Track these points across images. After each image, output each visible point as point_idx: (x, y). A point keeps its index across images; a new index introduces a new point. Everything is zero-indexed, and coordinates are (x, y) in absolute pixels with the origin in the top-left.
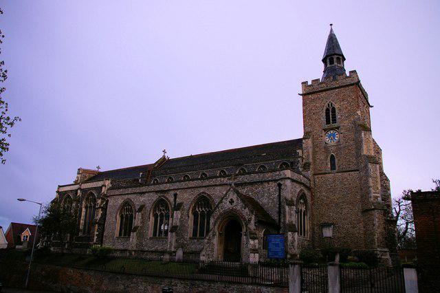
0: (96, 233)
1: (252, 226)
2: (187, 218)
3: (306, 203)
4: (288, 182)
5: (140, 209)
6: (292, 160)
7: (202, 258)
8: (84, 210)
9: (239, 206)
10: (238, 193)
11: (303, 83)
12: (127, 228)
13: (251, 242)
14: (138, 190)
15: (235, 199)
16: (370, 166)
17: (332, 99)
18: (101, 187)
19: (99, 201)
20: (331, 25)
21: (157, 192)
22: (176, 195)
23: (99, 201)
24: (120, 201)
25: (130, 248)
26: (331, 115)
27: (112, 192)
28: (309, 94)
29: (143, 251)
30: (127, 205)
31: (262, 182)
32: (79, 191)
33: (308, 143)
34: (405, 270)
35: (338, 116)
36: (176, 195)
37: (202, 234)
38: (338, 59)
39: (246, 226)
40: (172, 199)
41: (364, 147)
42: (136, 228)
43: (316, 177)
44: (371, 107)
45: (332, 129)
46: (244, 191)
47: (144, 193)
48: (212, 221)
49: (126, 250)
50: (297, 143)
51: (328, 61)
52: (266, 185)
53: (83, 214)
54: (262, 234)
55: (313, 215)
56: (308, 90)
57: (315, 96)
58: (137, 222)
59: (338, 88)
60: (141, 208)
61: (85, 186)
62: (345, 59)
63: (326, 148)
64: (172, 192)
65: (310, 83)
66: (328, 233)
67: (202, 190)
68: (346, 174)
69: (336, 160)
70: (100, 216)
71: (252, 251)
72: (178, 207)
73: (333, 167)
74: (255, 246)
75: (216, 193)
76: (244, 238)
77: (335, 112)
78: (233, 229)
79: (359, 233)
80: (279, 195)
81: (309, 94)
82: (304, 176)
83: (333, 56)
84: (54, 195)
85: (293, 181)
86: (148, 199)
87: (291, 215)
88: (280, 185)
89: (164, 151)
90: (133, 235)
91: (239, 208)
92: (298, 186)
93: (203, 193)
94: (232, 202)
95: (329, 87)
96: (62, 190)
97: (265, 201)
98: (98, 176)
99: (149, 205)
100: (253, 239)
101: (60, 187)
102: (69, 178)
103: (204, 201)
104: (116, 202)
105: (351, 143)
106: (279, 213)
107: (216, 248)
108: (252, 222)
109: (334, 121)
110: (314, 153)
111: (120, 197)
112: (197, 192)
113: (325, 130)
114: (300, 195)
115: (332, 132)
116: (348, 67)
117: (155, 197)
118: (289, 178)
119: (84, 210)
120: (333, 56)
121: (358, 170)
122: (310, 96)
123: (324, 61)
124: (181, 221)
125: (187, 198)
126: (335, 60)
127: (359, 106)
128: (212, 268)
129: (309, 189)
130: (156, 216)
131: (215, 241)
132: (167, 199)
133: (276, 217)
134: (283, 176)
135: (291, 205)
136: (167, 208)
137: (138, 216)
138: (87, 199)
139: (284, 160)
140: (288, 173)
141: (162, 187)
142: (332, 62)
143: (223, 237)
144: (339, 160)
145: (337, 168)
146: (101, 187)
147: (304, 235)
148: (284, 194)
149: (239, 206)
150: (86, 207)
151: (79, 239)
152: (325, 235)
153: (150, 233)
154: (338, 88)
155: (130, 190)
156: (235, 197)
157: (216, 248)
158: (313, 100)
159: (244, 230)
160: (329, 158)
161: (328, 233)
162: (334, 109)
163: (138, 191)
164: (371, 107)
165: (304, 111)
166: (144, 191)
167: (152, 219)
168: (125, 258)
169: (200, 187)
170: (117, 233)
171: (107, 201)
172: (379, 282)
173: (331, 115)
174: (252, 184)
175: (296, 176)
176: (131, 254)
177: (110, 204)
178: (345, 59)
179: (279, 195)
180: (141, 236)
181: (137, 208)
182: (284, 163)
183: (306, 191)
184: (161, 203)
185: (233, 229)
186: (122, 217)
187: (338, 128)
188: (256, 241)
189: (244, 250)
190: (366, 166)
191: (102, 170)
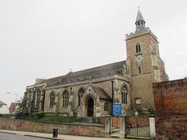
0: (41, 106)
1: (98, 100)
2: (76, 98)
3: (127, 89)
4: (116, 80)
5: (57, 95)
6: (121, 70)
7: (78, 115)
8: (36, 96)
9: (92, 92)
10: (92, 87)
11: (126, 35)
12: (52, 103)
13: (97, 108)
14: (56, 87)
15: (91, 89)
16: (155, 70)
17: (138, 41)
18: (42, 86)
19: (42, 92)
20: (139, 7)
21: (64, 87)
22: (71, 88)
23: (42, 92)
24: (50, 92)
25: (53, 112)
26: (138, 48)
27: (47, 88)
28: (129, 39)
29: (59, 113)
30: (52, 94)
31: (105, 81)
32: (34, 88)
33: (128, 62)
34: (150, 118)
35: (141, 49)
36: (71, 88)
37: (66, 105)
38: (142, 23)
39: (96, 101)
40: (70, 90)
41: (153, 62)
42: (56, 103)
43: (133, 77)
44: (159, 43)
45: (139, 55)
46: (98, 85)
47: (59, 88)
48: (82, 99)
49: (52, 113)
50: (124, 62)
51: (137, 24)
52: (107, 82)
53: (36, 98)
54: (103, 104)
55: (131, 94)
56: (128, 38)
57: (131, 40)
58: (56, 101)
59: (141, 36)
60: (59, 94)
61: (36, 86)
62: (145, 22)
63: (137, 64)
64: (70, 87)
65: (129, 35)
66: (138, 102)
67: (81, 86)
68: (145, 75)
69: (141, 69)
70: (42, 99)
71: (99, 111)
72: (72, 93)
73: (140, 71)
74: (99, 109)
75: (85, 86)
76: (95, 106)
77: (140, 47)
78: (90, 102)
79: (152, 102)
80: (113, 86)
81: (129, 39)
82: (126, 77)
83: (140, 23)
84: (25, 91)
85: (119, 79)
86: (60, 91)
87: (117, 95)
88: (112, 82)
89: (71, 69)
90: (55, 106)
91: (92, 93)
92: (122, 82)
93: (82, 87)
94: (90, 90)
95: (136, 36)
96: (28, 88)
97: (107, 89)
98: (44, 81)
99: (61, 93)
100: (98, 106)
101: (27, 87)
102: (32, 83)
103: (82, 90)
104: (48, 93)
105: (148, 60)
106: (113, 94)
107: (84, 111)
108: (98, 99)
109: (140, 51)
110: (131, 66)
111: (50, 90)
112: (79, 87)
113: (136, 55)
114: (123, 85)
115: (139, 56)
116: (146, 25)
117: (63, 90)
118: (116, 79)
119: (36, 96)
120: (140, 23)
121: (150, 73)
122: (129, 41)
123: (136, 24)
124: (73, 100)
125: (76, 89)
126: (140, 23)
127: (150, 43)
128: (81, 120)
129: (129, 83)
130: (64, 97)
131: (84, 108)
132: (68, 90)
133: (111, 96)
134: (114, 78)
135: (117, 91)
136: (68, 94)
137: (56, 98)
138: (38, 91)
139: (118, 70)
140: (116, 76)
141: (66, 85)
142: (139, 24)
143: (87, 106)
144: (142, 69)
145: (142, 72)
146: (42, 86)
147: (126, 104)
148: (114, 86)
149: (92, 92)
150: (37, 95)
151: (34, 109)
152: (137, 103)
153: (61, 105)
154: (141, 36)
155: (53, 87)
156: (90, 88)
157: (84, 111)
158: (130, 43)
159: (95, 102)
160: (138, 68)
161: (138, 102)
162: (139, 45)
163: (57, 87)
164: (159, 43)
165: (127, 48)
166: (59, 87)
167: (62, 99)
168: (52, 116)
169: (81, 84)
170: (49, 105)
171: (45, 92)
172: (144, 125)
173: (138, 48)
174: (101, 82)
175: (120, 77)
176: (54, 114)
177: (46, 93)
178: (145, 22)
179: (113, 86)
180: (58, 107)
181: (56, 94)
182: (118, 72)
183: (127, 84)
184: (65, 92)
185: (90, 102)
186: (51, 98)
187: (141, 54)
188: (99, 107)
189: (95, 111)
190: (153, 71)
191: (46, 79)
